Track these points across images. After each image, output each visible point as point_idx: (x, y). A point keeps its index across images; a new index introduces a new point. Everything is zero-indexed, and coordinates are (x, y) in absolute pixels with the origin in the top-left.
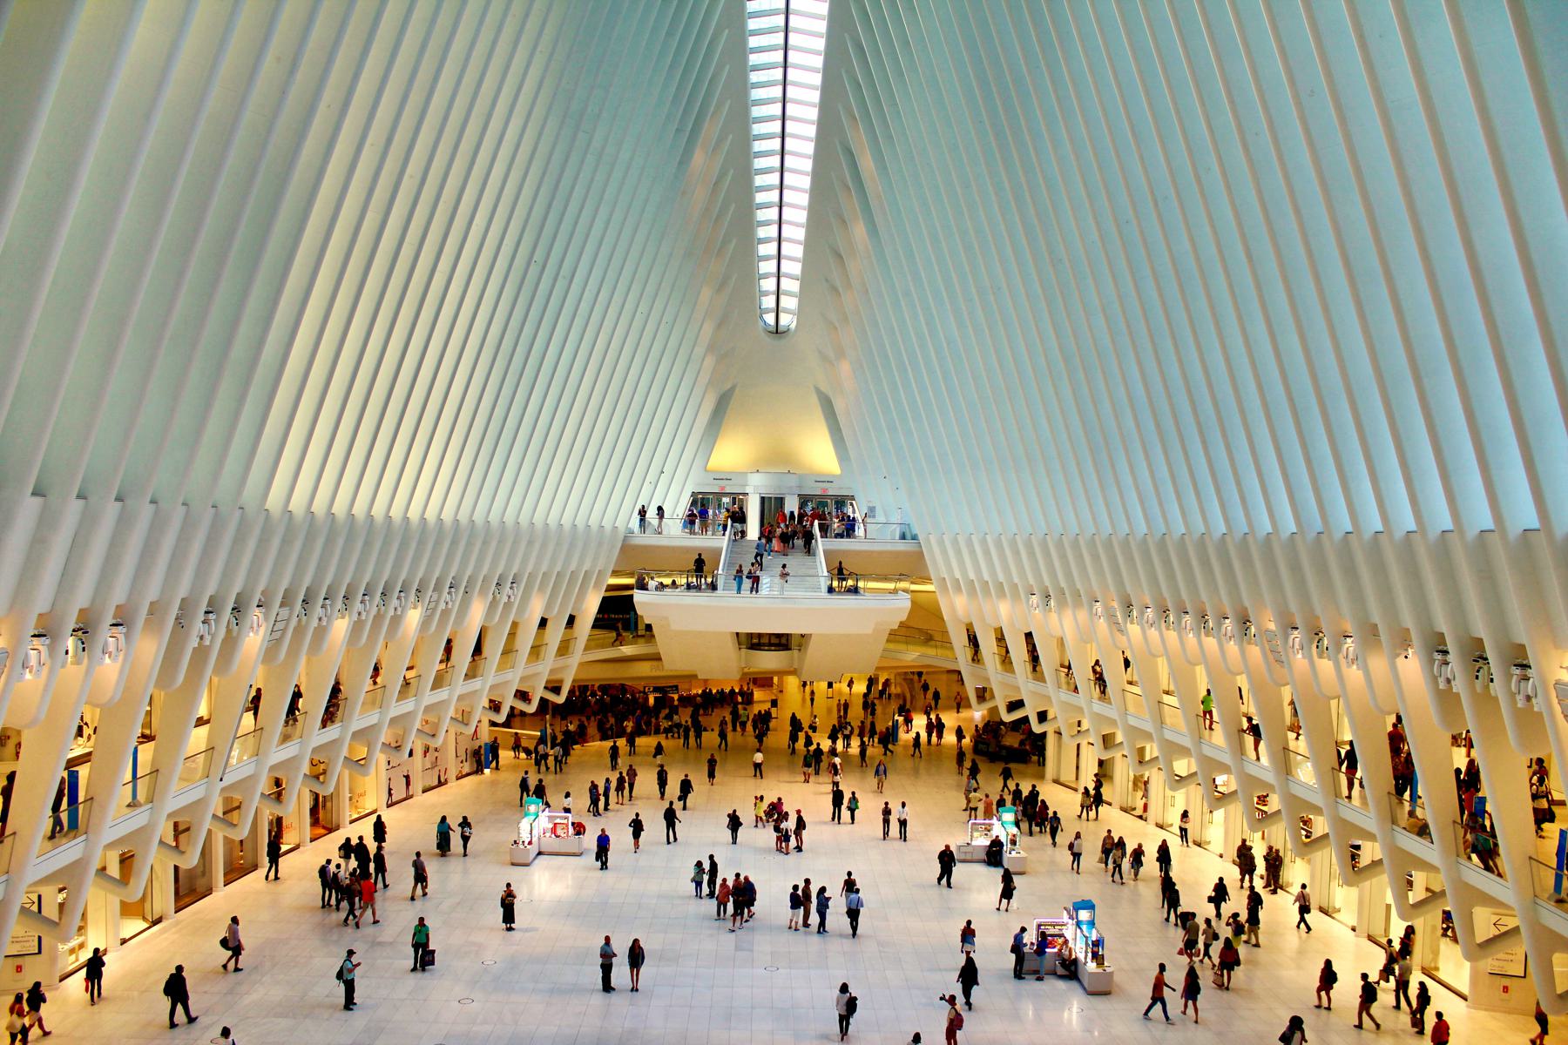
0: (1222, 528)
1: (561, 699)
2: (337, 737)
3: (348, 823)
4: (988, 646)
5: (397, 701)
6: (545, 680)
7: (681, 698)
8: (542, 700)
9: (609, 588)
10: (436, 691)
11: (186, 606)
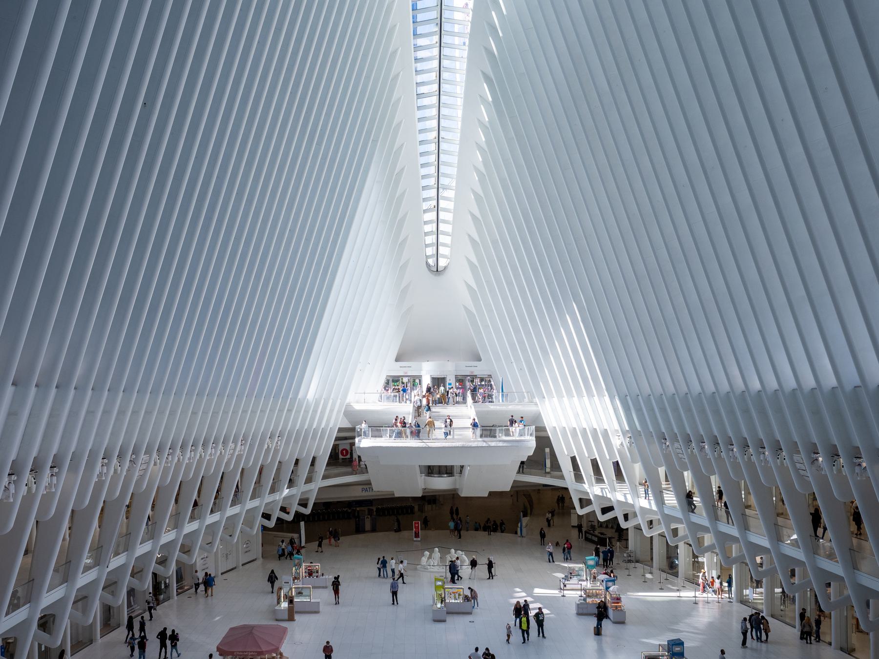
0: (712, 389)
1: (307, 511)
2: (218, 519)
3: (241, 565)
4: (586, 470)
5: (210, 515)
6: (298, 499)
7: (378, 509)
8: (279, 519)
9: (337, 439)
10: (232, 508)
11: (93, 455)
